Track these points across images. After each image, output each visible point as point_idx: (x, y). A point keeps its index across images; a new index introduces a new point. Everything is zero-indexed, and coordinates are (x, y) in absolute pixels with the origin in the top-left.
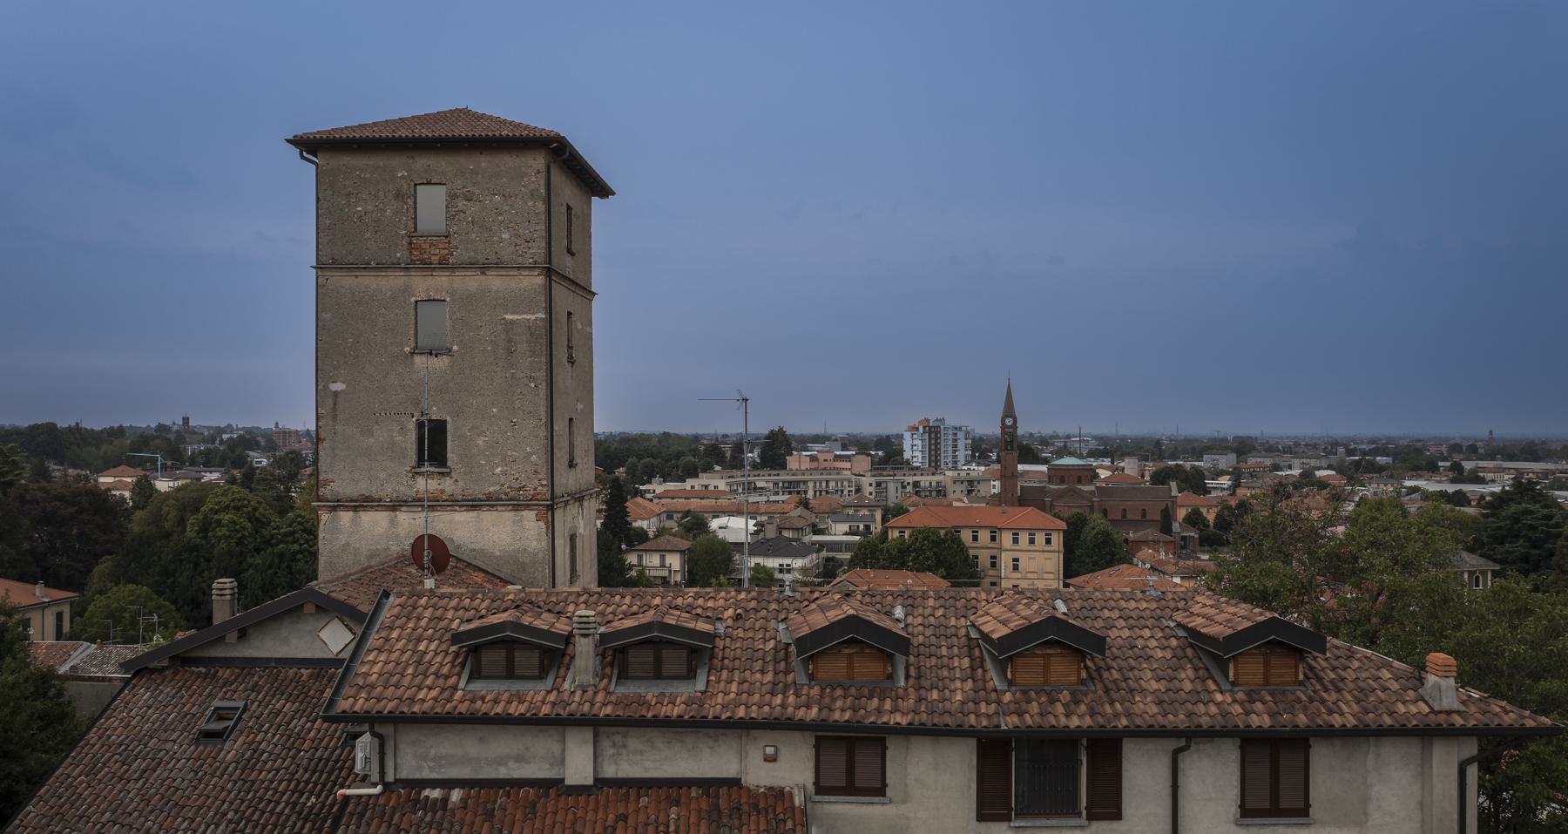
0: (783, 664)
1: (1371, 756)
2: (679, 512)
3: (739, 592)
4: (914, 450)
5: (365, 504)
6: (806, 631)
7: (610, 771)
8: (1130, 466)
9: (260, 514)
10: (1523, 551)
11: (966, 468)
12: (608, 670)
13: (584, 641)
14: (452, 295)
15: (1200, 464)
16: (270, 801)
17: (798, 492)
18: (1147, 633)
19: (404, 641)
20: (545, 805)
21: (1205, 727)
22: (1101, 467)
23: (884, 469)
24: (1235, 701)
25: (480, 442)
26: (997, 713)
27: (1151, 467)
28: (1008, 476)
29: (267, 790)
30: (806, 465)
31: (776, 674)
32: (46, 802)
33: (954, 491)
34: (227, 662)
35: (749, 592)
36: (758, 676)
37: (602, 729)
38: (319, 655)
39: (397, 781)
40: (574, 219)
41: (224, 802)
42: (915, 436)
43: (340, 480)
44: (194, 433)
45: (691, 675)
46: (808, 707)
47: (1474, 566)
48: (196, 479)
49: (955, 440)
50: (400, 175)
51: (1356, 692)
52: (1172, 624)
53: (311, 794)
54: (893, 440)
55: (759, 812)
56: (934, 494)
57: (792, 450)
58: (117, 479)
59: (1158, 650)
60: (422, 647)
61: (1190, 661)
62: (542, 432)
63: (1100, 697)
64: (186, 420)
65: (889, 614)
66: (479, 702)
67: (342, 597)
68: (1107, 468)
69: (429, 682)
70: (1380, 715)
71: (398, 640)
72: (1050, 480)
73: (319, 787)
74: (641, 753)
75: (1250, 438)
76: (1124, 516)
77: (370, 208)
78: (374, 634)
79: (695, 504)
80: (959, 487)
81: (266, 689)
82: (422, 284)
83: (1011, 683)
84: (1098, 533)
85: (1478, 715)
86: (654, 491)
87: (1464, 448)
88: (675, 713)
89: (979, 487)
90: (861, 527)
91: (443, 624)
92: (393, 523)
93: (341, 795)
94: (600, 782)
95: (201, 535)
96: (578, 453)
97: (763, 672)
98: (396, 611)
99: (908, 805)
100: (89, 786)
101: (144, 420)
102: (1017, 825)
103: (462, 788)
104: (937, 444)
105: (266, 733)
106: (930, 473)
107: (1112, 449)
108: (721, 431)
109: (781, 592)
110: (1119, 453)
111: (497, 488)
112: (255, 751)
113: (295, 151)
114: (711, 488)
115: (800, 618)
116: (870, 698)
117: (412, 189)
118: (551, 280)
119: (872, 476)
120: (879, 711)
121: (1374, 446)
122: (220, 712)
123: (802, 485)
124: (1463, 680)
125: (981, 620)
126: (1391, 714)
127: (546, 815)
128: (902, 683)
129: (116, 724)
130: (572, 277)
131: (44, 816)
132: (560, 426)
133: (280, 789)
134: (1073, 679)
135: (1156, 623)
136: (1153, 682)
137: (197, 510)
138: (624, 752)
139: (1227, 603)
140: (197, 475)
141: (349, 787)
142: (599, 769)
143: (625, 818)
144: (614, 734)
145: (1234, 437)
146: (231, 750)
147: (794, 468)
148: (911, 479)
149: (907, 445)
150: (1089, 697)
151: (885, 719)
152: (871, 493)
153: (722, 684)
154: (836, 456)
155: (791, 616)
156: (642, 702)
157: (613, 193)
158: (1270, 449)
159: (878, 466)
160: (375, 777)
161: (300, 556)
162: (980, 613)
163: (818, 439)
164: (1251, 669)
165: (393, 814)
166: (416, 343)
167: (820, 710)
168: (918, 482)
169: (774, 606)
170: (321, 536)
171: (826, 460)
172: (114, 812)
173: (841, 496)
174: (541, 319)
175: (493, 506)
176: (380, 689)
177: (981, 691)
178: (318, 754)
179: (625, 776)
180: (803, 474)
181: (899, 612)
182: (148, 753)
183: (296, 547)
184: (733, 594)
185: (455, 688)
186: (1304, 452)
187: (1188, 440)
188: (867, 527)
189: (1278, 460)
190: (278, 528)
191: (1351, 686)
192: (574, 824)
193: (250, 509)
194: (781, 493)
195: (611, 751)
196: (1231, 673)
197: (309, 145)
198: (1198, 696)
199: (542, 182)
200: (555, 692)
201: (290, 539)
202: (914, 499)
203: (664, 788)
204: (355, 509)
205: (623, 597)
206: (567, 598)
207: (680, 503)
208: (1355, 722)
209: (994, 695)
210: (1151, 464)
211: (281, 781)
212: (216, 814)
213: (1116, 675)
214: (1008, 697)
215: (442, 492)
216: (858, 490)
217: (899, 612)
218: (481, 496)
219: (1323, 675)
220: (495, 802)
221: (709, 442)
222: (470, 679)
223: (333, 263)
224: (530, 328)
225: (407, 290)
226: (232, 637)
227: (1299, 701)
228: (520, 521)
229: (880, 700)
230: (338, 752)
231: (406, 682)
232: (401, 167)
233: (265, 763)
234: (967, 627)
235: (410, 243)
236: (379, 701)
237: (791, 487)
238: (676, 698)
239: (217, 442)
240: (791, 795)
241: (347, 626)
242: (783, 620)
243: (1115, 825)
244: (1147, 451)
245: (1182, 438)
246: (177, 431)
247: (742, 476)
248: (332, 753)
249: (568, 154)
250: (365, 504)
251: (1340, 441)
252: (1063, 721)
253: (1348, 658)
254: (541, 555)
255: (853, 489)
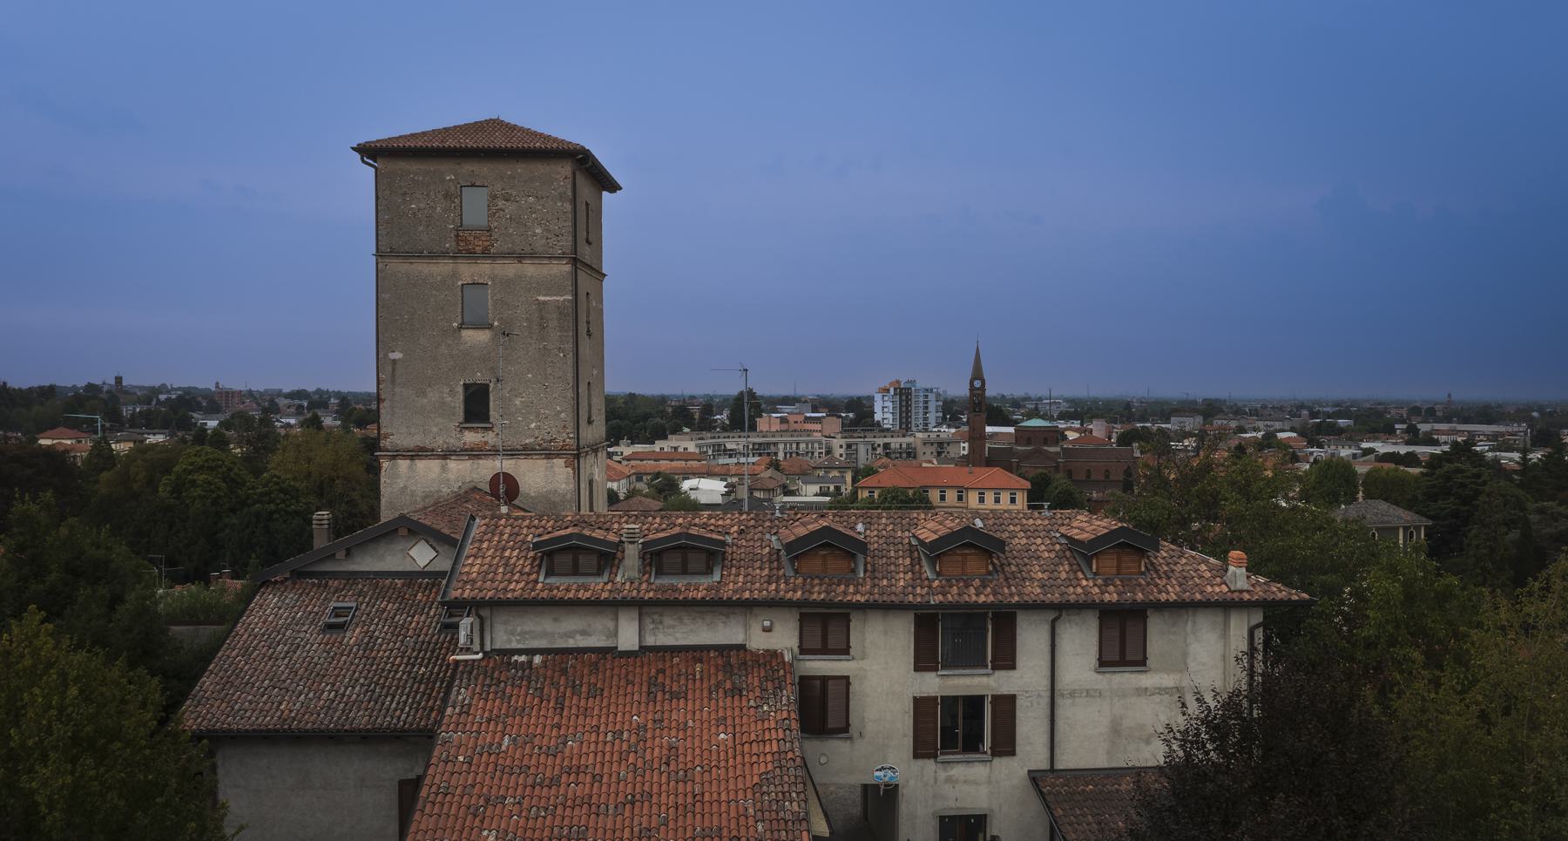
0: (776, 563)
1: (1190, 624)
2: (649, 474)
3: (741, 514)
4: (884, 412)
5: (420, 453)
6: (793, 538)
7: (650, 641)
8: (1098, 428)
9: (235, 474)
10: (1453, 507)
11: (936, 429)
12: (648, 568)
13: (631, 546)
14: (493, 280)
15: (1169, 426)
16: (390, 671)
17: (769, 454)
18: (1039, 541)
19: (492, 550)
20: (604, 665)
21: (1072, 602)
22: (1069, 429)
23: (854, 431)
24: (1095, 585)
25: (518, 403)
26: (928, 594)
27: (1118, 429)
28: (977, 438)
29: (386, 663)
30: (776, 426)
31: (771, 570)
32: (216, 675)
33: (924, 453)
34: (335, 575)
35: (748, 514)
36: (758, 571)
37: (645, 610)
38: (409, 568)
39: (492, 650)
40: (590, 213)
41: (355, 672)
42: (886, 398)
43: (397, 431)
44: (127, 393)
45: (709, 571)
46: (795, 591)
47: (1408, 522)
48: (139, 442)
49: (926, 402)
50: (448, 178)
51: (1180, 579)
52: (1058, 535)
53: (421, 666)
54: (864, 402)
55: (760, 665)
56: (904, 455)
57: (763, 411)
58: (55, 441)
59: (1046, 552)
60: (507, 554)
61: (1068, 559)
62: (570, 394)
63: (1001, 583)
64: (119, 380)
65: (853, 528)
66: (555, 591)
67: (427, 523)
68: (1076, 430)
69: (516, 577)
70: (1194, 593)
71: (487, 550)
72: (1017, 442)
73: (426, 661)
74: (673, 627)
75: (1219, 400)
76: (1088, 476)
77: (422, 205)
78: (468, 546)
79: (664, 465)
80: (929, 449)
81: (370, 593)
82: (468, 271)
83: (938, 574)
84: (1060, 492)
85: (1261, 593)
86: (622, 453)
87: (1423, 411)
88: (699, 596)
89: (949, 449)
90: (832, 488)
91: (519, 538)
92: (444, 469)
93: (453, 660)
94: (644, 649)
95: (174, 495)
96: (594, 411)
97: (761, 568)
98: (483, 528)
99: (865, 661)
100: (246, 663)
101: (71, 376)
102: (942, 673)
103: (541, 655)
104: (908, 406)
105: (377, 625)
106: (900, 434)
107: (1081, 411)
108: (688, 392)
109: (773, 514)
110: (1088, 415)
111: (532, 440)
112: (371, 638)
113: (358, 156)
114: (681, 450)
115: (787, 532)
116: (839, 585)
117: (458, 191)
118: (576, 268)
119: (842, 438)
120: (845, 593)
121: (1337, 409)
122: (338, 611)
123: (772, 446)
124: (1253, 569)
125: (919, 532)
126: (1202, 593)
127: (606, 670)
128: (862, 575)
129: (256, 620)
130: (589, 263)
131: (218, 684)
132: (583, 388)
133: (397, 663)
134: (983, 571)
135: (1046, 534)
136: (1039, 573)
137: (168, 471)
138: (661, 627)
139: (1096, 519)
140: (140, 437)
141: (458, 655)
142: (643, 640)
143: (663, 671)
144: (653, 614)
145: (1203, 400)
146: (352, 637)
147: (765, 430)
148: (881, 441)
149: (878, 407)
150: (993, 584)
151: (849, 598)
152: (841, 455)
153: (732, 577)
154: (806, 418)
155: (780, 531)
156: (675, 589)
157: (621, 189)
158: (1237, 411)
159: (849, 428)
160: (476, 647)
161: (276, 516)
162: (919, 527)
163: (787, 401)
164: (1109, 564)
165: (493, 672)
166: (463, 319)
167: (803, 593)
168: (889, 444)
169: (768, 524)
170: (382, 480)
171: (796, 422)
172: (271, 680)
173: (811, 458)
174: (568, 300)
175: (529, 455)
176: (480, 583)
177: (918, 578)
178: (420, 639)
179: (661, 644)
180: (773, 436)
181: (860, 527)
182: (287, 640)
183: (272, 506)
184: (737, 515)
185: (536, 582)
186: (1270, 415)
187: (1157, 403)
188: (838, 489)
189: (1243, 423)
190: (253, 488)
191: (1178, 575)
192: (627, 676)
193: (225, 469)
194: (751, 455)
195: (651, 626)
196: (1094, 567)
197: (368, 152)
198: (1069, 582)
199: (569, 186)
200: (610, 584)
201: (267, 498)
202: (884, 460)
203: (691, 652)
204: (412, 458)
205: (654, 518)
206: (612, 519)
207: (649, 465)
208: (1175, 598)
209: (926, 582)
210: (1119, 426)
211: (396, 658)
212: (350, 680)
213: (1013, 568)
214: (936, 583)
215: (486, 443)
216: (829, 452)
217: (860, 527)
218: (518, 447)
219: (1159, 568)
220: (567, 663)
221: (677, 404)
222: (547, 575)
223: (391, 252)
224: (559, 307)
225: (455, 275)
226: (341, 554)
227: (1140, 585)
228: (552, 467)
229: (846, 586)
230: (436, 637)
231: (499, 577)
232: (449, 172)
233: (381, 645)
234: (909, 537)
235: (457, 236)
236: (481, 591)
237: (760, 449)
238: (700, 586)
239: (154, 403)
240: (782, 655)
241: (431, 546)
242: (775, 534)
243: (1011, 673)
244: (1116, 413)
245: (1153, 400)
246: (109, 392)
247: (711, 438)
248: (431, 638)
249: (590, 163)
250: (420, 453)
251: (1306, 403)
252: (974, 598)
253: (1180, 557)
254: (569, 496)
255: (823, 451)
